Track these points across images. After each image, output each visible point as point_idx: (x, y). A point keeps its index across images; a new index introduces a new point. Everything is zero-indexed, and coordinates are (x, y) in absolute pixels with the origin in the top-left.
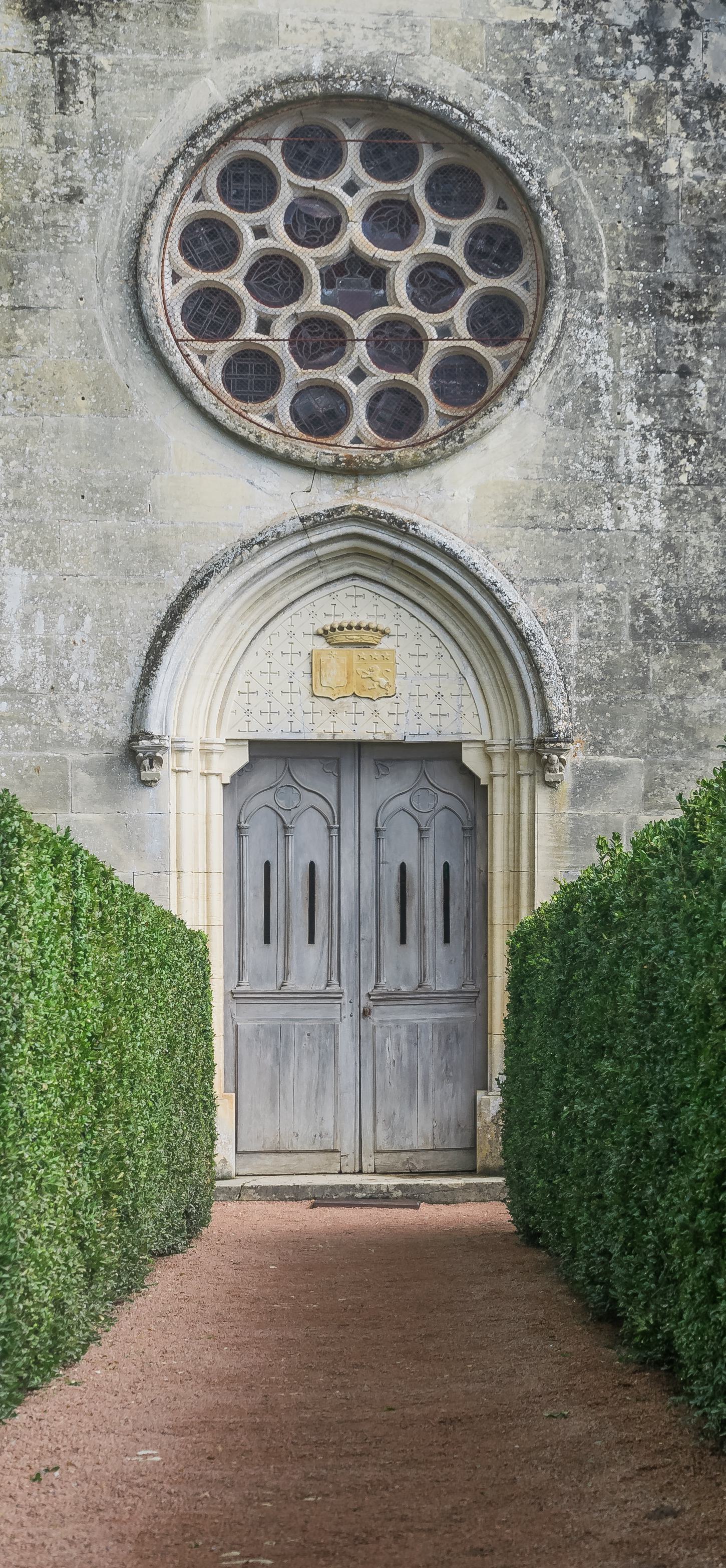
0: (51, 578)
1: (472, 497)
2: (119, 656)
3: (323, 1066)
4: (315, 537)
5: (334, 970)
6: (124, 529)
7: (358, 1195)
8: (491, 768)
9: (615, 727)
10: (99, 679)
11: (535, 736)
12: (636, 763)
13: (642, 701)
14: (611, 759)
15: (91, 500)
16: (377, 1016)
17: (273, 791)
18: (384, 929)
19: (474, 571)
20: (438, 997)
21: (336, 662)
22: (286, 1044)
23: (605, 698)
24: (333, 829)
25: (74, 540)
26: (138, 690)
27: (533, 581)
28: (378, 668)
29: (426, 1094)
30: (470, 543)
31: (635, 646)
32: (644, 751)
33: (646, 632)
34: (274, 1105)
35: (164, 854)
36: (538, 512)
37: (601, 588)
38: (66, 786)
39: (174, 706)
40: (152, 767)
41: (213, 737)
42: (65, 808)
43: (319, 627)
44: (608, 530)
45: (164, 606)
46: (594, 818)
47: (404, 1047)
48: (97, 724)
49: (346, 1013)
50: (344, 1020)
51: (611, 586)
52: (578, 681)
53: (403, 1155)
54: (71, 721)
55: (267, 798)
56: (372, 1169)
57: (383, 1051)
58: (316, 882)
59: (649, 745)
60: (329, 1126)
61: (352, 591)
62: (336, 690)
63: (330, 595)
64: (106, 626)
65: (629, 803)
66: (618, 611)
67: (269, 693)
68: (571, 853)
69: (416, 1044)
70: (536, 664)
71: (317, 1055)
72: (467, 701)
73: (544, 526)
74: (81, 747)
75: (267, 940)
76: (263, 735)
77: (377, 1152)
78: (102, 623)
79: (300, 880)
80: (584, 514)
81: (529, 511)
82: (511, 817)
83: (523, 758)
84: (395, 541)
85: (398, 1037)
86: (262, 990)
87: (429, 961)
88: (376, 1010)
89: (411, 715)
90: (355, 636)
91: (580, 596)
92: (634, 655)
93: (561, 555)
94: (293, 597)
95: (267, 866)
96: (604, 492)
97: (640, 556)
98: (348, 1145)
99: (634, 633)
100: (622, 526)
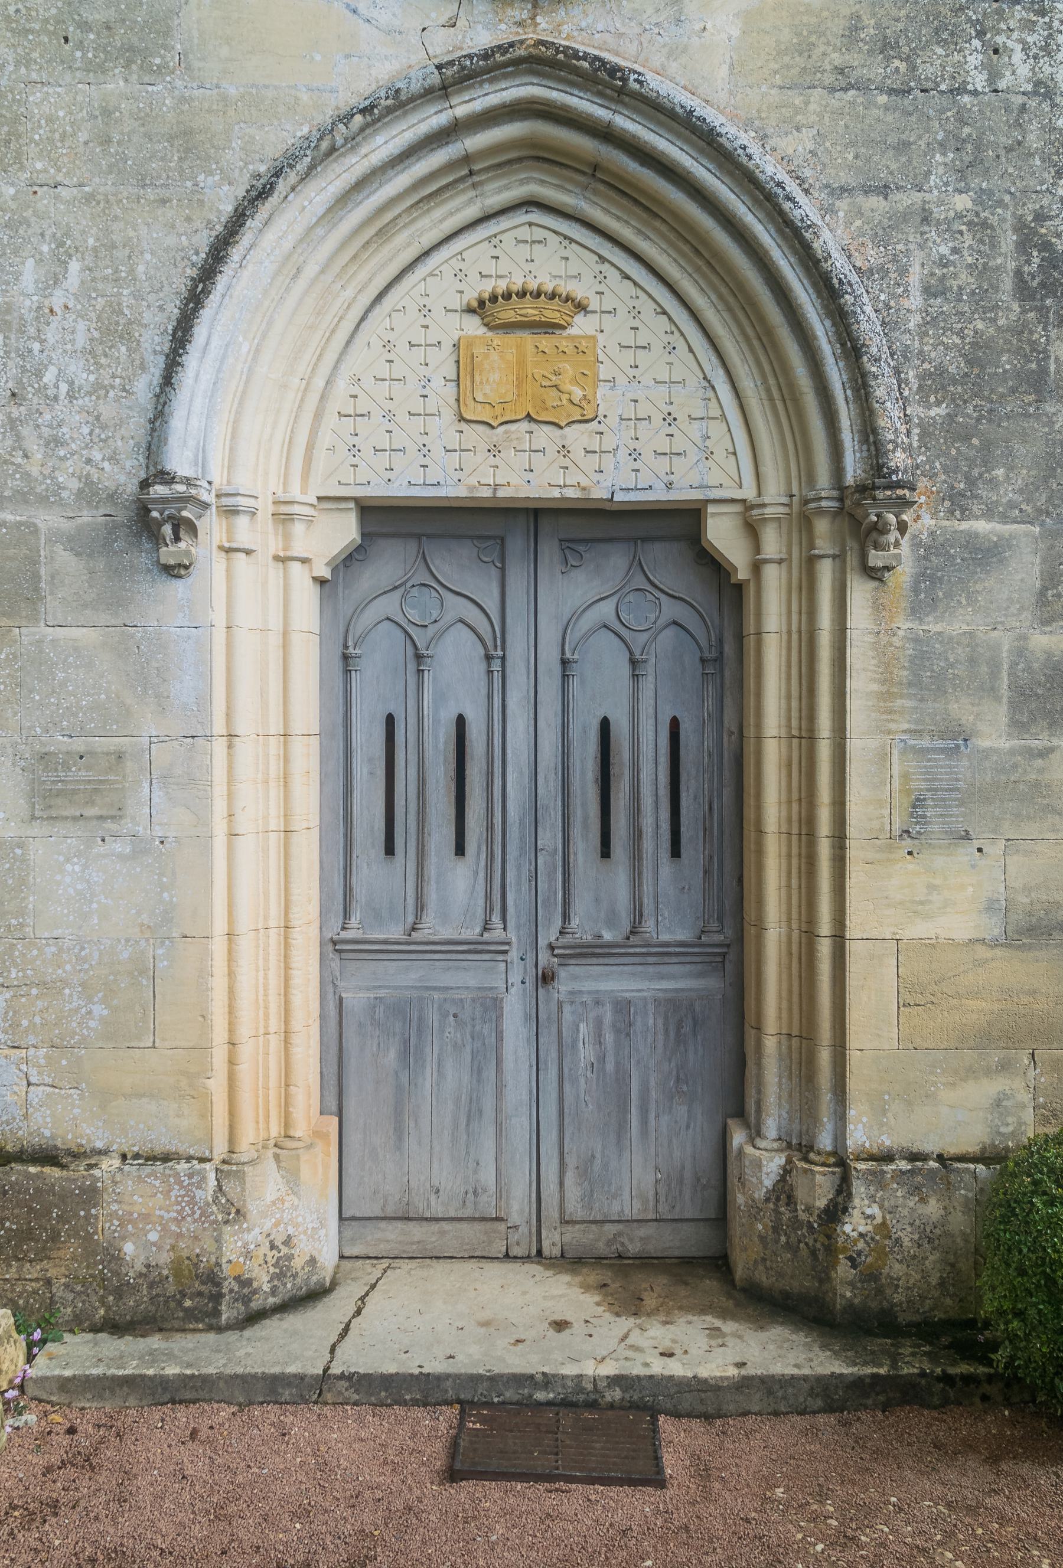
0: (12, 191)
1: (736, 33)
2: (127, 336)
3: (477, 1071)
4: (465, 105)
5: (495, 903)
6: (136, 99)
7: (540, 1396)
8: (757, 548)
9: (987, 465)
10: (92, 378)
11: (849, 480)
12: (1027, 534)
13: (1037, 417)
14: (981, 526)
15: (80, 46)
16: (563, 986)
17: (398, 594)
18: (576, 832)
19: (744, 160)
20: (665, 954)
21: (501, 359)
22: (420, 1032)
23: (970, 410)
24: (494, 658)
25: (50, 120)
26: (158, 396)
27: (843, 189)
28: (569, 370)
29: (644, 1122)
30: (733, 118)
31: (1024, 312)
32: (1039, 511)
33: (1043, 285)
34: (400, 1139)
35: (204, 700)
36: (854, 59)
37: (962, 202)
38: (36, 577)
39: (220, 431)
40: (177, 539)
41: (295, 493)
42: (34, 618)
43: (471, 296)
44: (975, 93)
45: (203, 241)
46: (951, 638)
47: (609, 1038)
48: (89, 461)
49: (515, 978)
50: (513, 990)
51: (983, 198)
52: (922, 377)
53: (608, 1227)
54: (46, 455)
55: (389, 605)
56: (556, 1251)
57: (575, 1041)
58: (468, 750)
59: (1049, 499)
60: (488, 1176)
61: (524, 233)
62: (498, 409)
63: (489, 239)
64: (105, 278)
65: (1013, 609)
66: (993, 246)
67: (390, 415)
68: (911, 703)
69: (628, 1035)
70: (853, 340)
71: (468, 1049)
72: (717, 429)
73: (861, 86)
74: (61, 503)
75: (390, 850)
76: (378, 490)
77: (565, 1222)
78: (97, 274)
79: (441, 746)
80: (933, 64)
81: (837, 59)
82: (795, 637)
83: (822, 526)
84: (602, 113)
85: (599, 1023)
86: (382, 937)
87: (647, 888)
88: (563, 974)
89: (622, 453)
90: (529, 310)
91: (926, 218)
92: (1021, 330)
93: (892, 139)
94: (429, 239)
95: (390, 720)
96: (969, 20)
97: (1034, 141)
98: (519, 1208)
99: (1023, 290)
100: (1002, 85)
